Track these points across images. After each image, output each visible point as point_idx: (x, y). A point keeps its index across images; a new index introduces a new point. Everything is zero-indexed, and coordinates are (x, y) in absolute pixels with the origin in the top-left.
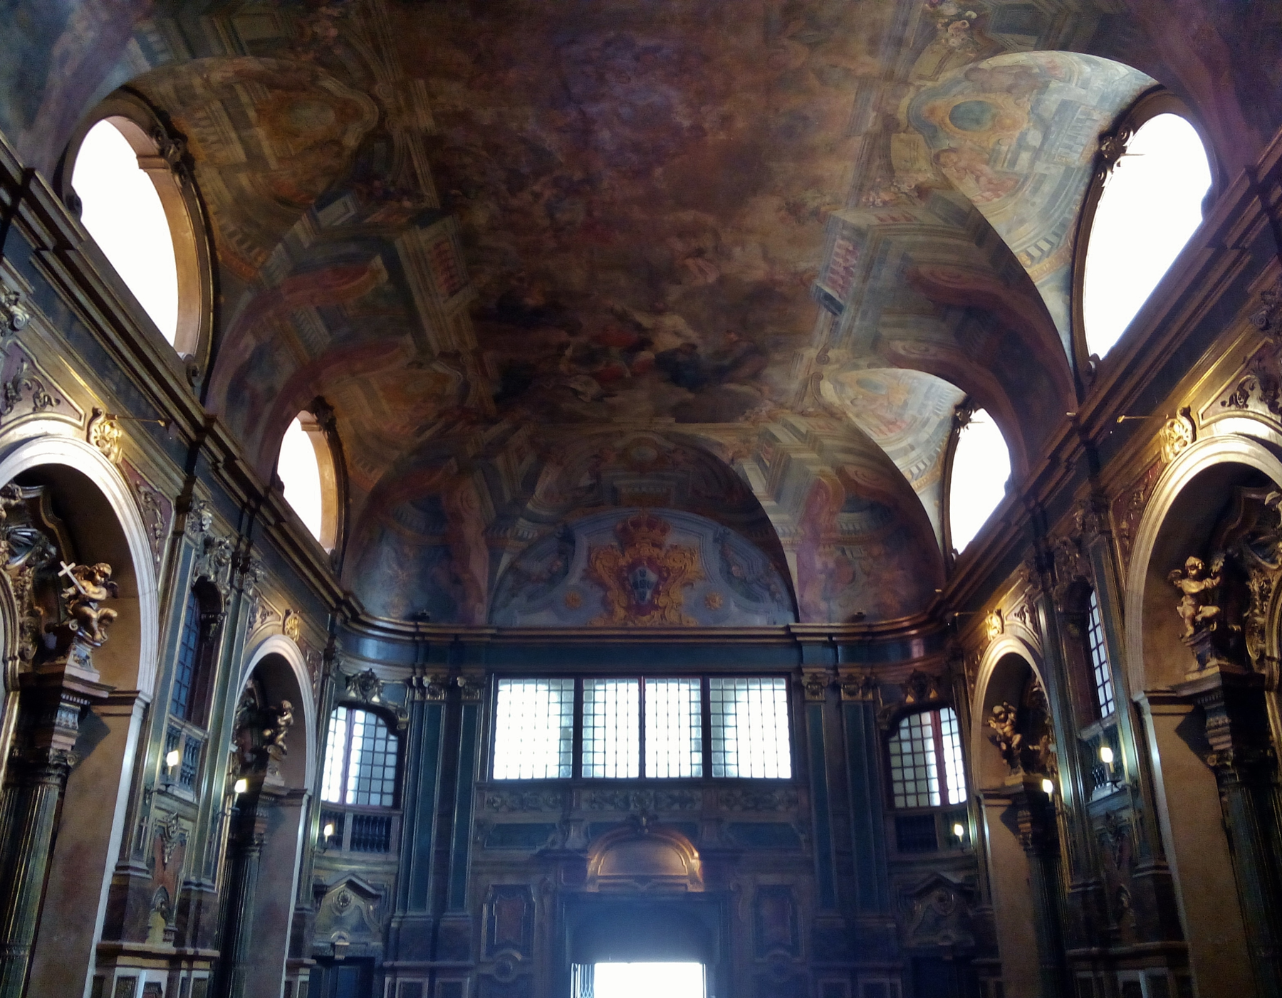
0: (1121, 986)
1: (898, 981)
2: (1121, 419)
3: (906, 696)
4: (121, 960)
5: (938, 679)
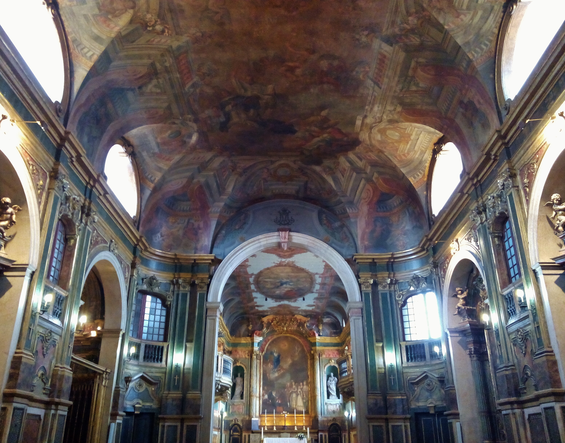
0: (526, 417)
1: (408, 424)
2: (527, 121)
3: (410, 287)
4: (16, 399)
5: (426, 278)
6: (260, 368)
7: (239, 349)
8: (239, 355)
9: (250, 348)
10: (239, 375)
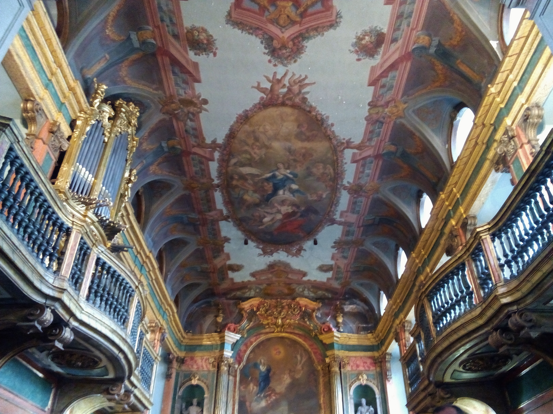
6: (234, 391)
7: (198, 354)
8: (197, 365)
9: (217, 353)
10: (195, 401)
